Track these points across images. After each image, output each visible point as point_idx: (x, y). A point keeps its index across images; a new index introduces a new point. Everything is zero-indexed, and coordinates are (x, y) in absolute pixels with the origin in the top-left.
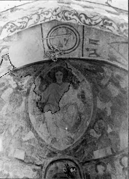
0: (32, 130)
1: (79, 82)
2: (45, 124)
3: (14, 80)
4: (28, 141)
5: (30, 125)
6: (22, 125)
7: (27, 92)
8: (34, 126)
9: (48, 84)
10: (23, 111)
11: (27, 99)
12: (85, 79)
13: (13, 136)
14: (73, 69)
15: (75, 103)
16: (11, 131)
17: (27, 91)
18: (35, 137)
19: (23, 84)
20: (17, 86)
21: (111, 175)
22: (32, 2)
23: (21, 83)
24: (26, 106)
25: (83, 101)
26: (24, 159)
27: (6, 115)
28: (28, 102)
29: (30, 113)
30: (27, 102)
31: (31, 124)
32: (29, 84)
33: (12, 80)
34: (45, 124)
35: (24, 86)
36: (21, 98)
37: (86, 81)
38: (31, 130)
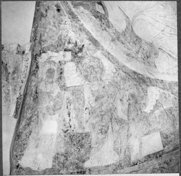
0: (149, 84)
3: (57, 52)
4: (156, 106)
5: (142, 79)
6: (131, 91)
7: (92, 42)
13: (129, 120)
16: (119, 114)
17: (90, 43)
18: (162, 91)
19: (74, 42)
20: (70, 52)
21: (44, 169)
23: (69, 43)
26: (164, 147)
27: (96, 100)
28: (109, 53)
29: (127, 62)
30: (107, 54)
31: (141, 76)
32: (79, 32)
33: (55, 54)
35: (78, 41)
36: (95, 58)
38: (148, 85)
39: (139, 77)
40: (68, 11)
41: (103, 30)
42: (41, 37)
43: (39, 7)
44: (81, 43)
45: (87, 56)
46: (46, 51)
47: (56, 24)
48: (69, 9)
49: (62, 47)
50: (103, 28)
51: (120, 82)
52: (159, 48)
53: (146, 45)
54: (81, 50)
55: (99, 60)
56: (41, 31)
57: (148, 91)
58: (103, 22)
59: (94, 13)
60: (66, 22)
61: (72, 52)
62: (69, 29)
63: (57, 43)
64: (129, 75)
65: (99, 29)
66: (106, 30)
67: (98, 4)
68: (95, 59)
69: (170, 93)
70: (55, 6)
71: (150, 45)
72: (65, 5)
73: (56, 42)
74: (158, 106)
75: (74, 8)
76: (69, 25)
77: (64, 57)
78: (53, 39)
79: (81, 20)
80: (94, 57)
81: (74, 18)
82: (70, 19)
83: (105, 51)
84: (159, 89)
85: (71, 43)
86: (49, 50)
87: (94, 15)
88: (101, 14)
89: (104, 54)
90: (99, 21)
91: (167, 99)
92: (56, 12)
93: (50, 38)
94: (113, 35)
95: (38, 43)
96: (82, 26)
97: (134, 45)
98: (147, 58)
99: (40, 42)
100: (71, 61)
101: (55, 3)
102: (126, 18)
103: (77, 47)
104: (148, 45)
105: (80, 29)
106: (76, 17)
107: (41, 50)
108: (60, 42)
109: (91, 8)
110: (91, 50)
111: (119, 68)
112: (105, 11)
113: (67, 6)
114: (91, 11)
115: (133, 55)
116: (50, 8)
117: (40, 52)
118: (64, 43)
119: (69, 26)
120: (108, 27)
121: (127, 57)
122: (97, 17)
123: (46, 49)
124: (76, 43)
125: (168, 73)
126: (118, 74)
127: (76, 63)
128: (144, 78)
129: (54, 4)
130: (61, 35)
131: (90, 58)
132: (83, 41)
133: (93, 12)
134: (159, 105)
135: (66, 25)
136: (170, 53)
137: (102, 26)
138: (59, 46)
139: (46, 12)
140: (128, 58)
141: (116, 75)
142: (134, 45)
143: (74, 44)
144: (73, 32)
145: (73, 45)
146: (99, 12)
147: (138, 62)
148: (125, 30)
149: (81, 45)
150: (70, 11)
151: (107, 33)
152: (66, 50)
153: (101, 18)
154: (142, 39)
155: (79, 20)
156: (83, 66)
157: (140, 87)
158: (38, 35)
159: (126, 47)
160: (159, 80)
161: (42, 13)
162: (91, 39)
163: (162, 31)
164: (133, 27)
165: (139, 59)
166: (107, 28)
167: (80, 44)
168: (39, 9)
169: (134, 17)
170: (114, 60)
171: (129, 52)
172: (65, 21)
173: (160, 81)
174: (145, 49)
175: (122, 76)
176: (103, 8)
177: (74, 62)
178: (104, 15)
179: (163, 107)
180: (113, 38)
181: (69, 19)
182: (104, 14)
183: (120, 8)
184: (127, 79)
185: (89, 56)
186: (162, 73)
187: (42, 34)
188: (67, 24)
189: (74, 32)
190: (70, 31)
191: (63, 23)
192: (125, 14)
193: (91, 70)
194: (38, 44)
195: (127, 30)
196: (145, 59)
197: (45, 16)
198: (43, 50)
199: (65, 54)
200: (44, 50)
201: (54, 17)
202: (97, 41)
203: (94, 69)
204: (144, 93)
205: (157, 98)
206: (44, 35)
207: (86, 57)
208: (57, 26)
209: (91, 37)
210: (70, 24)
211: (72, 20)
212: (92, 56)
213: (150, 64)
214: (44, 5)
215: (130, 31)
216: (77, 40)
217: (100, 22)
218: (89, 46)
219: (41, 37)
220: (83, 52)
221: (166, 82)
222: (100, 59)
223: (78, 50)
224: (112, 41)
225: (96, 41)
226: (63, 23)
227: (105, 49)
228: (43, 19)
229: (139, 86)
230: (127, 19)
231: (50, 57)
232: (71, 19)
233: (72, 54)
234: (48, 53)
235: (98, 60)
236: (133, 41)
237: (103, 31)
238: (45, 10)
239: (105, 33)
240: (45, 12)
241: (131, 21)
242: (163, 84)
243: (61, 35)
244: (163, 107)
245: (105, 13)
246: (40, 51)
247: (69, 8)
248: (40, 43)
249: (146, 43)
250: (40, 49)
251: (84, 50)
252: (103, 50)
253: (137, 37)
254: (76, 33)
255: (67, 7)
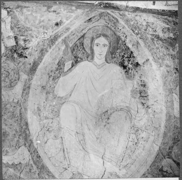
1: (137, 64)
2: (59, 141)
3: (12, 28)
5: (26, 134)
7: (33, 66)
8: (34, 137)
9: (77, 62)
10: (16, 101)
11: (29, 79)
12: (151, 58)
14: (129, 34)
15: (126, 108)
19: (27, 46)
20: (15, 44)
22: (4, 97)
23: (25, 41)
24: (24, 94)
25: (143, 104)
28: (29, 87)
30: (28, 86)
31: (28, 132)
34: (59, 141)
35: (30, 50)
37: (153, 63)
39: (26, 130)
40: (58, 34)
41: (48, 74)
42: (25, 7)
43: (58, 4)
44: (28, 54)
45: (17, 64)
46: (10, 15)
47: (42, 23)
48: (60, 35)
49: (18, 33)
50: (51, 74)
51: (9, 112)
52: (62, 138)
53: (57, 123)
54: (21, 55)
55: (18, 79)
56: (32, 7)
57: (20, 148)
58: (56, 72)
59: (62, 61)
60: (47, 34)
61: (15, 46)
62: (40, 38)
63: (22, 27)
64: (21, 120)
65: (48, 70)
66: (50, 77)
67: (71, 63)
68: (17, 74)
69: (37, 172)
70: (61, 21)
71: (59, 127)
72: (63, 30)
73: (23, 26)
74: (17, 168)
75: (62, 40)
76: (43, 37)
77: (7, 38)
78: (26, 22)
79: (52, 49)
80: (19, 73)
81: (52, 42)
82: (50, 37)
83: (30, 82)
84: (31, 158)
85: (25, 43)
86: (12, 18)
87: (60, 61)
88: (64, 69)
89: (25, 83)
90: (56, 68)
91: (30, 172)
92: (55, 22)
93: (27, 18)
94: (49, 86)
95: (18, 5)
96: (46, 52)
97: (51, 111)
98: (47, 129)
99: (20, 7)
100: (5, 47)
101: (63, 20)
102: (69, 94)
103: (23, 51)
104: (58, 125)
105: (42, 50)
106: (54, 44)
107: (10, 9)
108: (23, 30)
109: (66, 57)
110: (25, 67)
111: (20, 104)
112: (67, 71)
113: (63, 32)
114: (62, 57)
115: (42, 115)
116: (58, 15)
117: (7, 8)
118: (23, 35)
119: (43, 38)
120: (53, 78)
121: (36, 109)
122: (59, 64)
123: (12, 14)
124: (26, 49)
125: (50, 158)
126: (14, 107)
127: (6, 53)
128: (28, 136)
129: (62, 19)
130: (31, 30)
131: (16, 68)
132: (30, 55)
133: (63, 59)
134: (19, 168)
135: (43, 34)
136: (65, 150)
137: (51, 72)
138: (19, 30)
139: (53, 11)
140: (36, 110)
141: (13, 105)
142: (51, 111)
143: (25, 46)
144: (37, 43)
145: (24, 45)
146: (64, 66)
147: (38, 122)
148: (59, 97)
149: (26, 54)
150: (58, 36)
151: (48, 79)
152: (16, 38)
153: (60, 69)
154: (59, 117)
155: (50, 47)
156: (4, 62)
157: (17, 137)
158: (27, 4)
159: (45, 103)
160: (37, 153)
161: (52, 6)
162: (35, 64)
163: (77, 132)
164: (65, 104)
165: (41, 122)
166: (51, 79)
167: (27, 52)
168: (57, 4)
169: (74, 101)
170: (25, 96)
171: (42, 109)
172: (47, 33)
173: (37, 155)
174: (53, 123)
175: (16, 112)
176: (70, 69)
177: (5, 51)
178: (63, 71)
179: (20, 173)
180: (45, 87)
181: (50, 36)
182: (65, 71)
183: (75, 85)
184: (16, 119)
185: (17, 66)
186: (45, 152)
187: (29, 8)
188: (44, 35)
189: (38, 44)
190: (38, 40)
191: (45, 30)
192: (72, 91)
193: (4, 74)
194: (17, 5)
195: (60, 99)
196: (46, 128)
197: (49, 10)
198: (11, 11)
199: (11, 38)
200: (11, 12)
201: (49, 20)
202: (36, 71)
203: (6, 77)
204: (16, 145)
205: (22, 162)
206: (29, 11)
207: (15, 63)
208: (41, 24)
209: (37, 63)
210: (45, 38)
211: (49, 39)
212: (19, 71)
213: (45, 135)
214: (60, 8)
215: (61, 102)
216: (30, 49)
217: (55, 69)
218: (28, 64)
219: (25, 7)
220: (19, 58)
221: (42, 161)
222: (20, 80)
223: (19, 52)
224: (43, 87)
225: (35, 70)
226: (45, 30)
227: (31, 82)
228: (46, 8)
229: (18, 136)
230: (69, 96)
231: (5, 21)
232: (50, 39)
233: (13, 46)
234: (9, 17)
235: (18, 78)
236: (53, 108)
237: (47, 75)
238: (55, 10)
239: (46, 77)
240: (52, 9)
241: (69, 100)
242: (38, 159)
243: (31, 30)
244: (20, 173)
245: (65, 72)
246: (9, 8)
247: (61, 35)
248: (18, 7)
249: (59, 122)
250: (11, 7)
251: (21, 59)
252: (29, 80)
253: (59, 111)
254: (37, 46)
255: (61, 33)
